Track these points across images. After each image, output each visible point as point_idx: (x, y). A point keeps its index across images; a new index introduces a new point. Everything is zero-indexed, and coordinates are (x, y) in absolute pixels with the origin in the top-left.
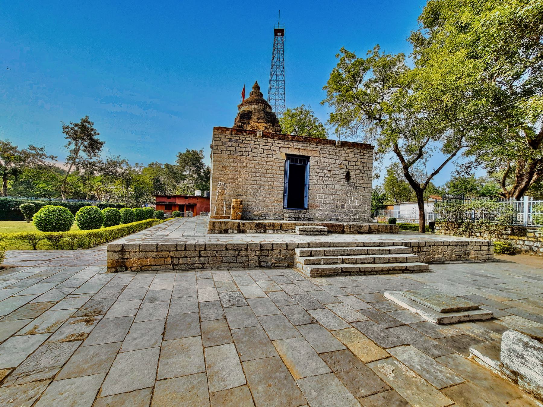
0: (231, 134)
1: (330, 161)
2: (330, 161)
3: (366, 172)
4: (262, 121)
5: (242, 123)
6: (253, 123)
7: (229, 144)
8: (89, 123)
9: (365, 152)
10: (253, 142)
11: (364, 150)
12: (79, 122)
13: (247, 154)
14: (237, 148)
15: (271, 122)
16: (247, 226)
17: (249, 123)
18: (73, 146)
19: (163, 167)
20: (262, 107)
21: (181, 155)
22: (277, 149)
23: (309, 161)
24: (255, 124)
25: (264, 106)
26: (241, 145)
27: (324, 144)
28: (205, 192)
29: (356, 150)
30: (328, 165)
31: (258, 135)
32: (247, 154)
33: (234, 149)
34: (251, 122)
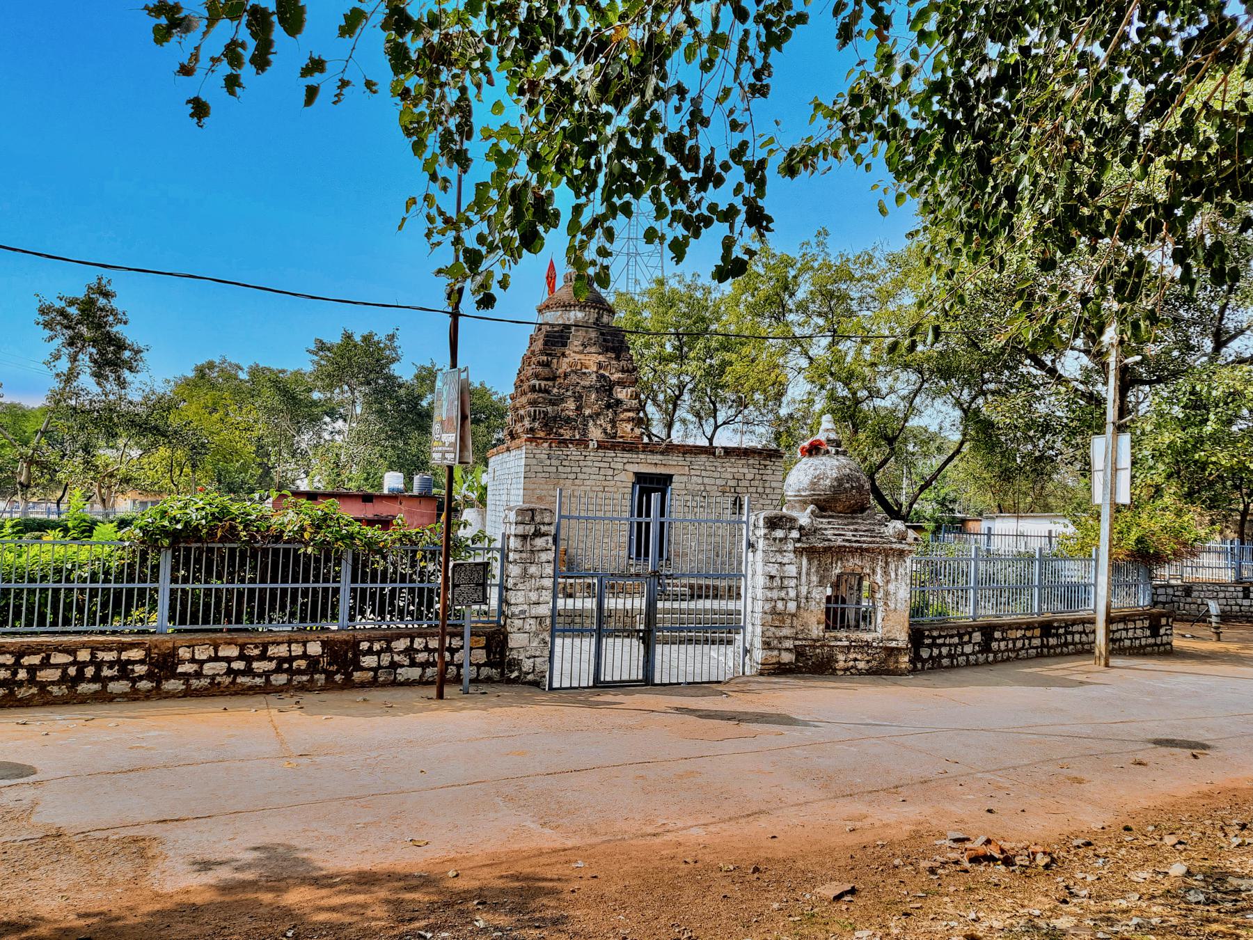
0: (550, 447)
1: (706, 481)
2: (706, 481)
3: (770, 497)
4: (593, 349)
5: (547, 355)
6: (572, 355)
7: (548, 462)
8: (106, 295)
9: (768, 463)
10: (582, 458)
11: (765, 459)
12: (81, 294)
13: (573, 476)
14: (560, 468)
15: (613, 350)
16: (578, 587)
17: (564, 355)
18: (64, 365)
19: (243, 376)
20: (593, 314)
21: (322, 346)
22: (620, 466)
23: (671, 482)
24: (578, 357)
25: (598, 313)
26: (565, 463)
27: (695, 454)
28: (417, 479)
29: (751, 462)
30: (703, 488)
31: (591, 446)
32: (573, 476)
33: (554, 469)
34: (567, 352)
